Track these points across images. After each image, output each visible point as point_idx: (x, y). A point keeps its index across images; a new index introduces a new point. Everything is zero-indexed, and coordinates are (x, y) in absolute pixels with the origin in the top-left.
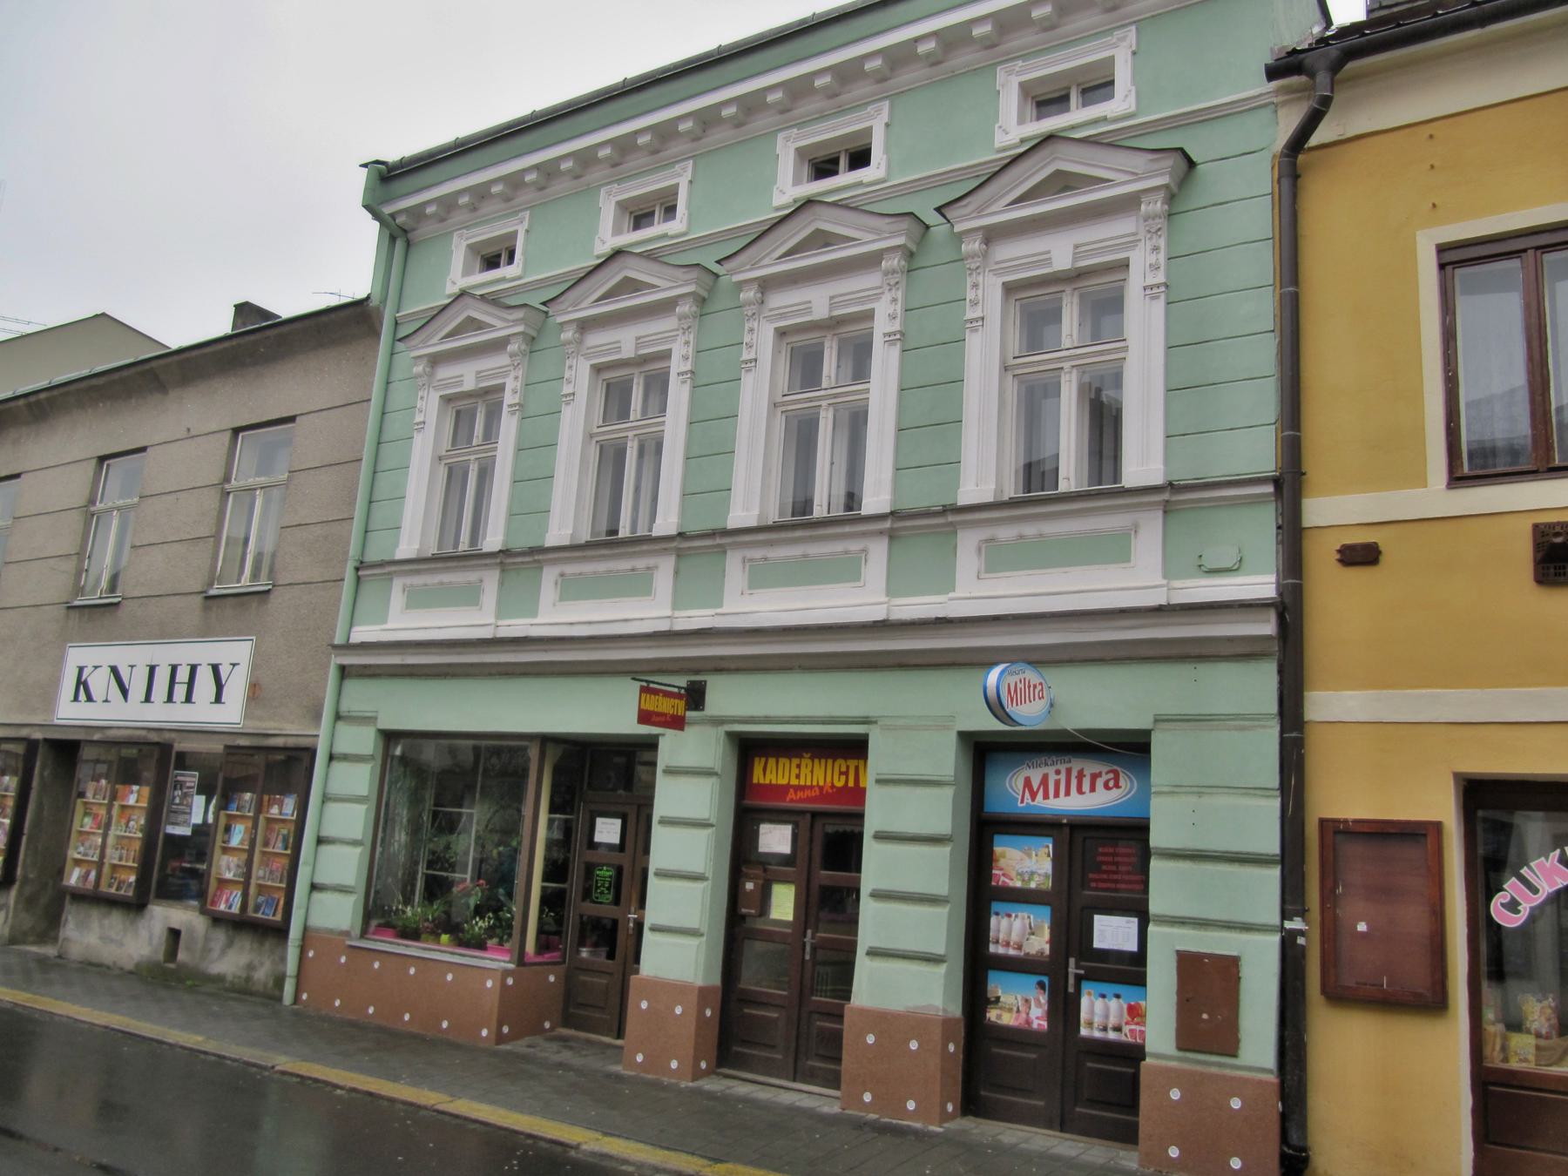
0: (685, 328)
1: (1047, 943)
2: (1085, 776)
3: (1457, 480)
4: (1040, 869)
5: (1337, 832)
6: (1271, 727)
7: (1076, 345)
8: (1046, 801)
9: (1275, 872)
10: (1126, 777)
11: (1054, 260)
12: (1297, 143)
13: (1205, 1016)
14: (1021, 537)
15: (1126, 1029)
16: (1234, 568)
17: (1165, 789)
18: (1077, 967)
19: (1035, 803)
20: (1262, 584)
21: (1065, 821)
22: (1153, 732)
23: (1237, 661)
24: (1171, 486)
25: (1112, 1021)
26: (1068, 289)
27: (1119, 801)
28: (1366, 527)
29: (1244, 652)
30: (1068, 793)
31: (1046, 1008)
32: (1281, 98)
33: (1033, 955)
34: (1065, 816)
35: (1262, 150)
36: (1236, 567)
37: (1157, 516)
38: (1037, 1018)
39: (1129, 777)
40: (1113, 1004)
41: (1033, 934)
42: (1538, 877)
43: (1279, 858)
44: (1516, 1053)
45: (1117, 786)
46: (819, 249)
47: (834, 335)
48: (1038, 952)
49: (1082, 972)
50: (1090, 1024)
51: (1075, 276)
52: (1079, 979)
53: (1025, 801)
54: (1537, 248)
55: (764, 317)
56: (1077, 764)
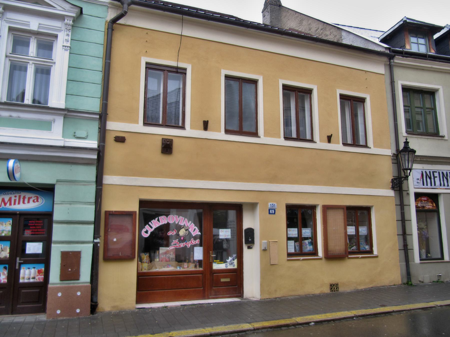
0: (68, 29)
1: (8, 253)
2: (26, 198)
3: (145, 124)
4: (6, 229)
5: (110, 214)
6: (94, 185)
7: (35, 56)
8: (11, 206)
9: (92, 226)
10: (41, 198)
11: (31, 25)
12: (114, 21)
13: (70, 270)
14: (11, 116)
15: (37, 278)
16: (85, 138)
17: (59, 202)
18: (20, 260)
19: (6, 207)
20: (93, 144)
21: (18, 213)
22: (56, 185)
23: (84, 165)
24: (67, 110)
25: (32, 276)
26: (33, 37)
27: (36, 207)
28: (340, 152)
29: (86, 163)
30: (19, 203)
31: (7, 275)
32: (110, 6)
33: (2, 258)
34: (18, 211)
35: (103, 18)
36: (86, 137)
37: (62, 118)
38: (3, 279)
39: (41, 198)
40: (33, 271)
41: (3, 251)
42: (152, 224)
43: (94, 222)
44: (144, 268)
45: (37, 201)
46: (32, 3)
47: (36, 38)
48: (4, 257)
49: (22, 261)
50: (24, 278)
51: (37, 34)
52: (20, 264)
53: (2, 206)
54: (167, 71)
55: (4, 20)
56: (23, 194)
